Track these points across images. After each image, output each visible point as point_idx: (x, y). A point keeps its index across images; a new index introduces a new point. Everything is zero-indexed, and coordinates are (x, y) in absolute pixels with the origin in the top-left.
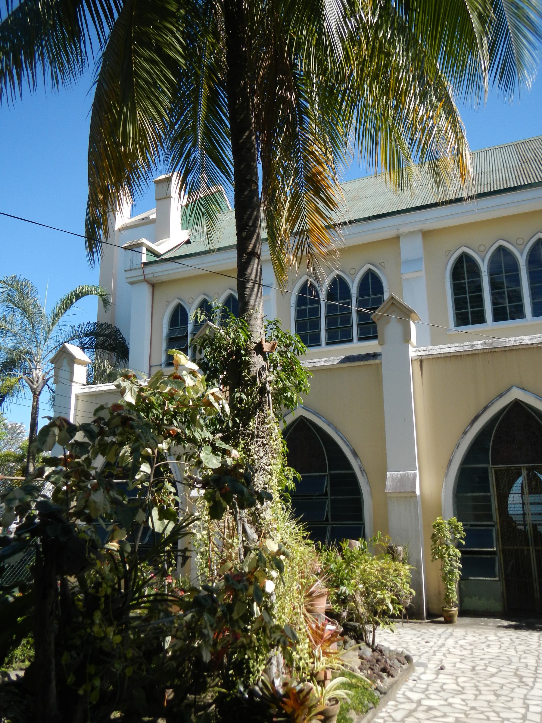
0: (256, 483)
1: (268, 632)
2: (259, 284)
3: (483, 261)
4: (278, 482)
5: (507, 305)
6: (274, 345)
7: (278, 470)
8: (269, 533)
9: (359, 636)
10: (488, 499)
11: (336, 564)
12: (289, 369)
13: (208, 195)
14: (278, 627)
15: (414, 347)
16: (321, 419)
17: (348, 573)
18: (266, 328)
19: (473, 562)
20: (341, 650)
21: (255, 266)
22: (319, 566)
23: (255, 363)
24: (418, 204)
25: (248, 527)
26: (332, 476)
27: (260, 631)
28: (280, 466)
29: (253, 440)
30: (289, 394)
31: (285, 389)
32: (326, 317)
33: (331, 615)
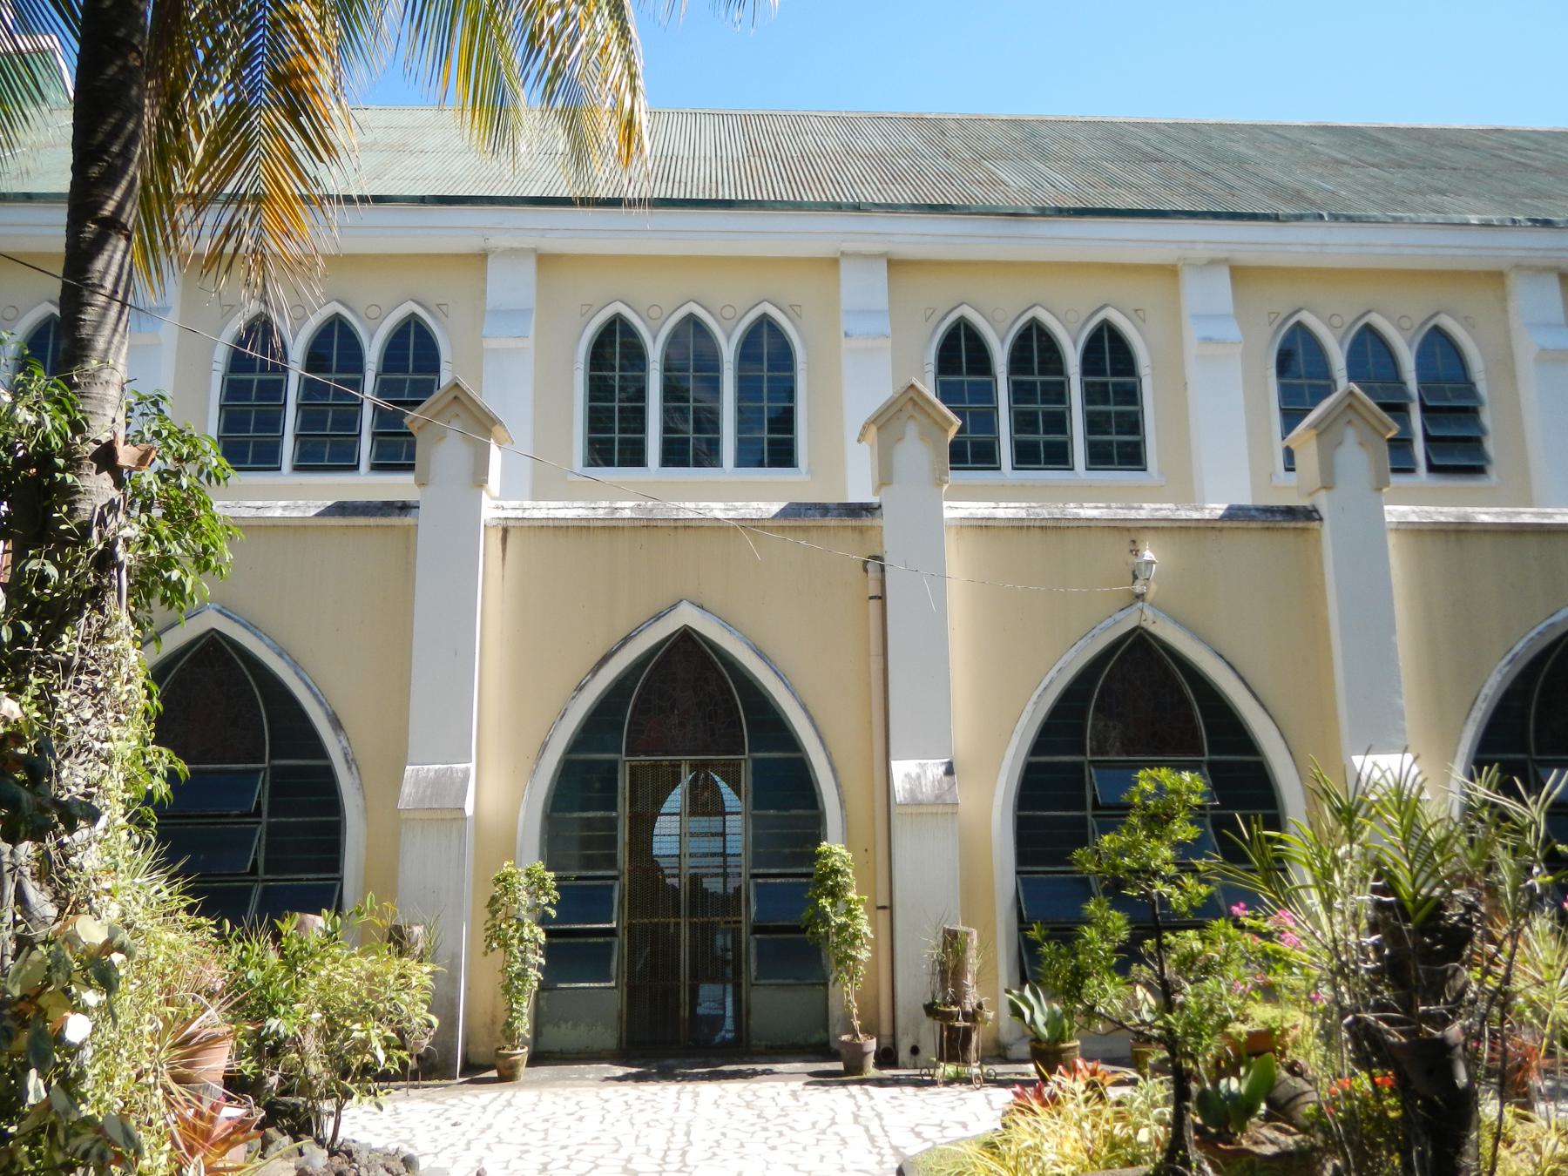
0: (64, 782)
1: (61, 1135)
2: (124, 304)
3: (728, 338)
4: (126, 780)
5: (691, 436)
6: (147, 454)
7: (129, 753)
8: (89, 901)
9: (301, 1125)
10: (612, 824)
11: (262, 968)
12: (182, 515)
13: (8, 54)
14: (88, 1122)
15: (493, 498)
16: (261, 639)
17: (289, 987)
18: (131, 410)
19: (568, 952)
20: (251, 1161)
21: (118, 256)
22: (215, 976)
23: (90, 492)
24: (535, 192)
25: (32, 891)
26: (756, 761)
27: (44, 1137)
28: (134, 743)
29: (65, 676)
30: (175, 575)
31: (166, 562)
32: (299, 406)
33: (235, 1084)
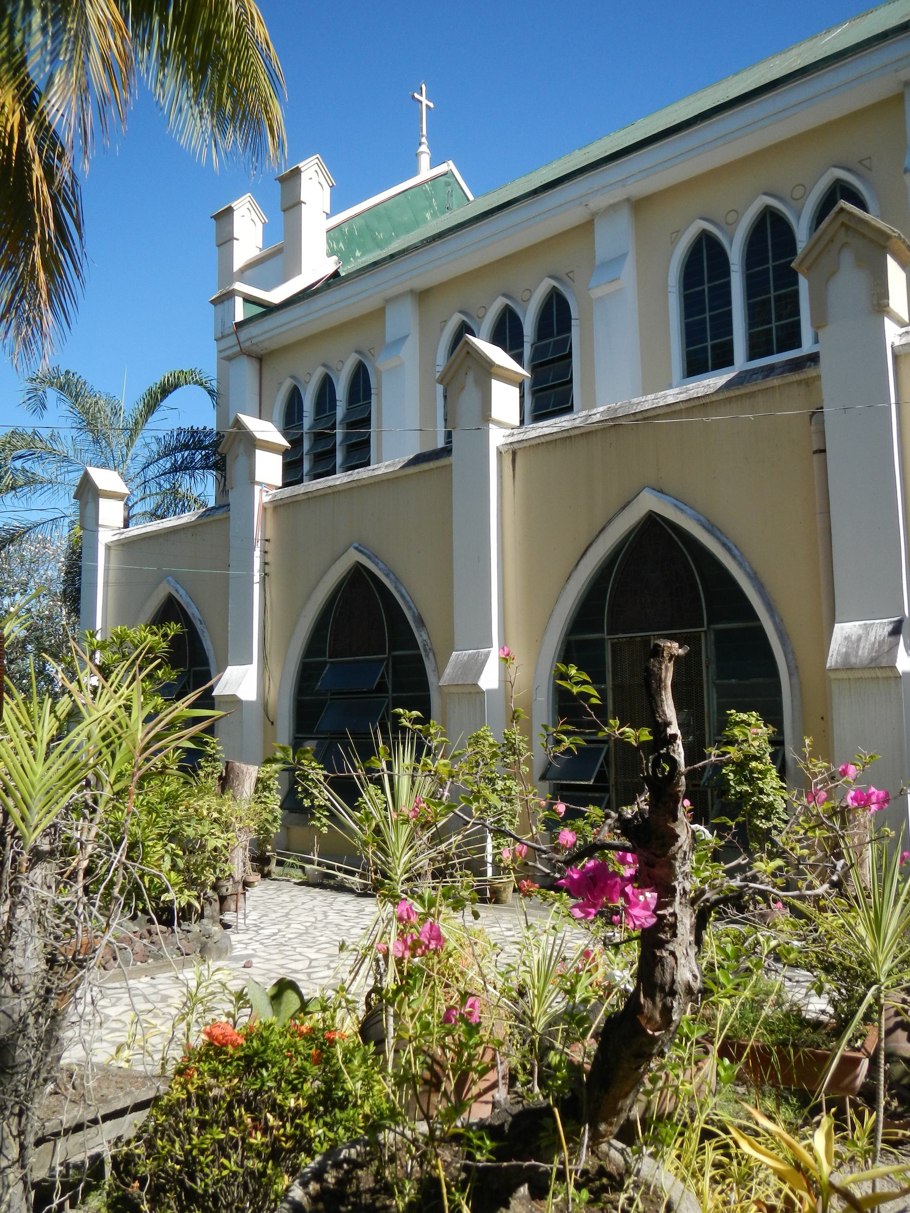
26: (718, 632)
